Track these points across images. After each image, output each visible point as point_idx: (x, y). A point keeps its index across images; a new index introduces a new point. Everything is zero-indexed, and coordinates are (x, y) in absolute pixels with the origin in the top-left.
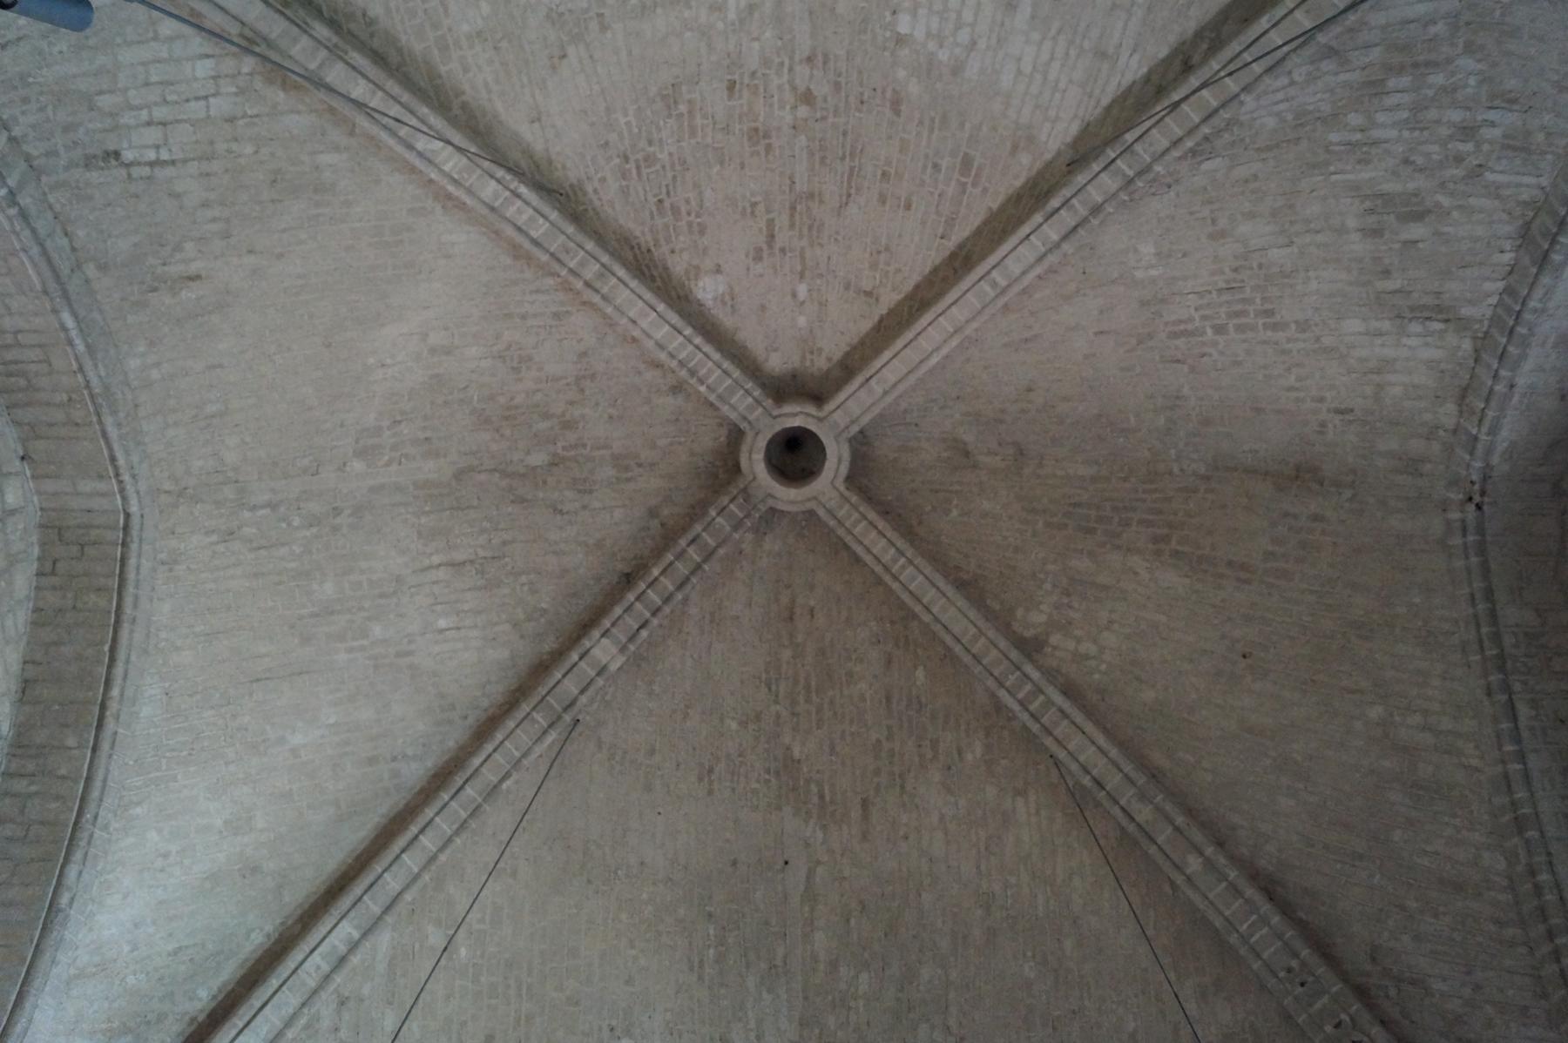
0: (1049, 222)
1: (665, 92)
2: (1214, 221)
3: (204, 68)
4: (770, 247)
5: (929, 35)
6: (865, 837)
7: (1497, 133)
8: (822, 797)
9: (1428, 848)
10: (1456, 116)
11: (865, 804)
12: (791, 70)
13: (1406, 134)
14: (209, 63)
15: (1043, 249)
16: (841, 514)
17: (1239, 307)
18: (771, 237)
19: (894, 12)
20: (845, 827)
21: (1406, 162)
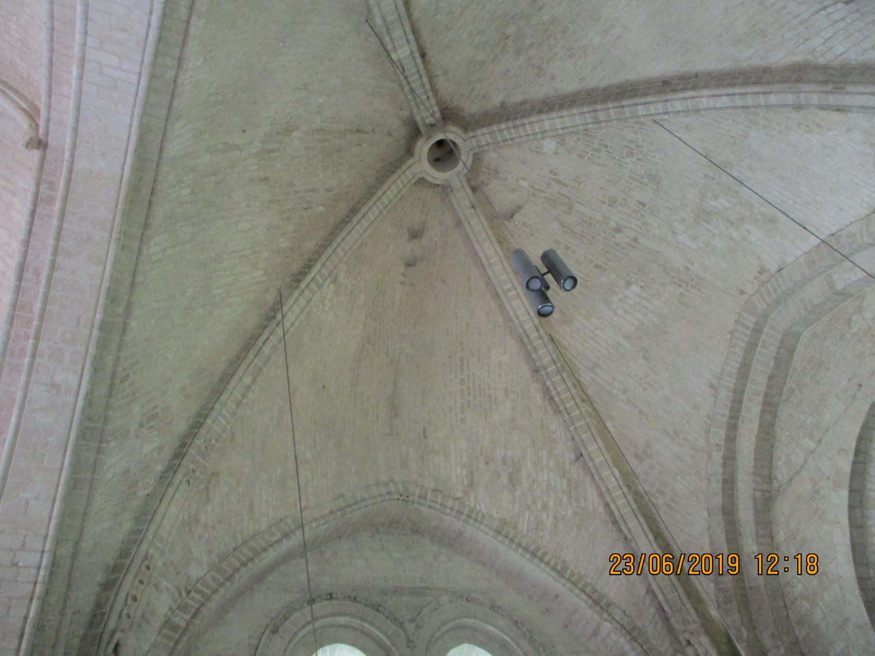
0: (534, 327)
1: (658, 178)
2: (513, 392)
3: (839, 49)
4: (554, 180)
5: (626, 297)
6: (252, 180)
7: (544, 519)
8: (272, 151)
9: (262, 491)
10: (551, 504)
11: (266, 179)
12: (635, 231)
13: (545, 483)
14: (839, 52)
15: (521, 320)
16: (408, 173)
17: (472, 393)
18: (559, 182)
19: (642, 287)
20: (256, 167)
21: (534, 481)
